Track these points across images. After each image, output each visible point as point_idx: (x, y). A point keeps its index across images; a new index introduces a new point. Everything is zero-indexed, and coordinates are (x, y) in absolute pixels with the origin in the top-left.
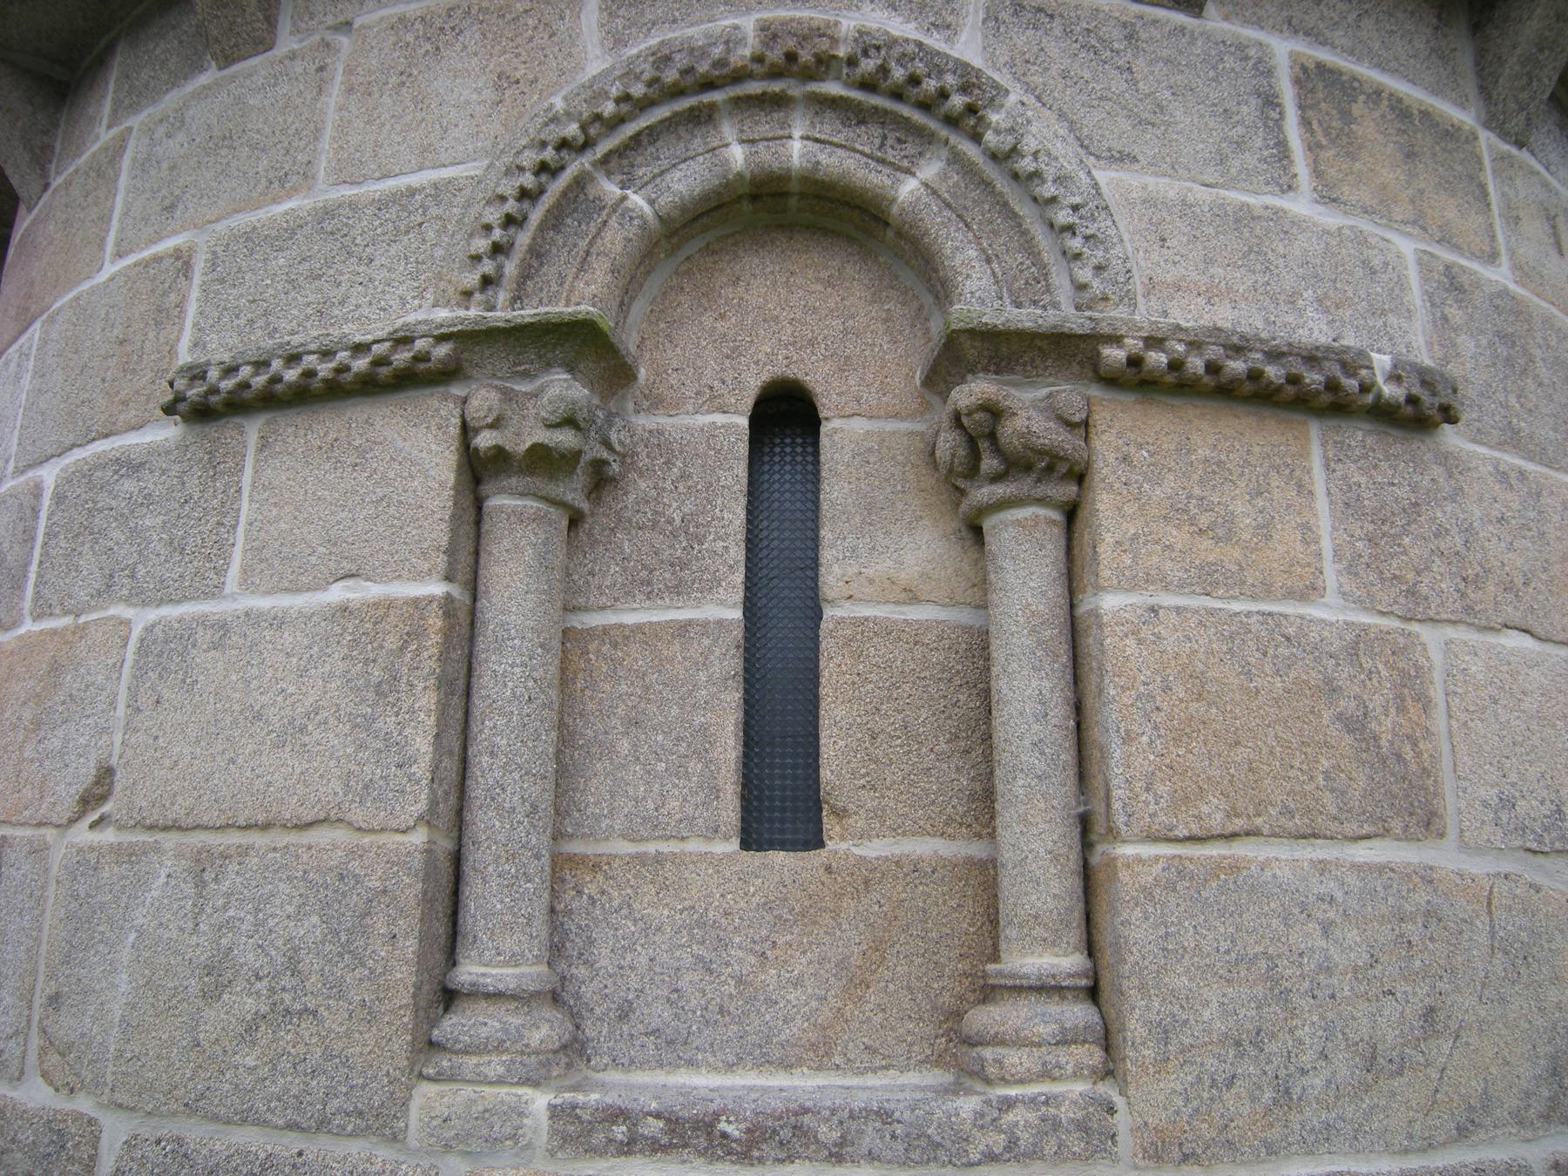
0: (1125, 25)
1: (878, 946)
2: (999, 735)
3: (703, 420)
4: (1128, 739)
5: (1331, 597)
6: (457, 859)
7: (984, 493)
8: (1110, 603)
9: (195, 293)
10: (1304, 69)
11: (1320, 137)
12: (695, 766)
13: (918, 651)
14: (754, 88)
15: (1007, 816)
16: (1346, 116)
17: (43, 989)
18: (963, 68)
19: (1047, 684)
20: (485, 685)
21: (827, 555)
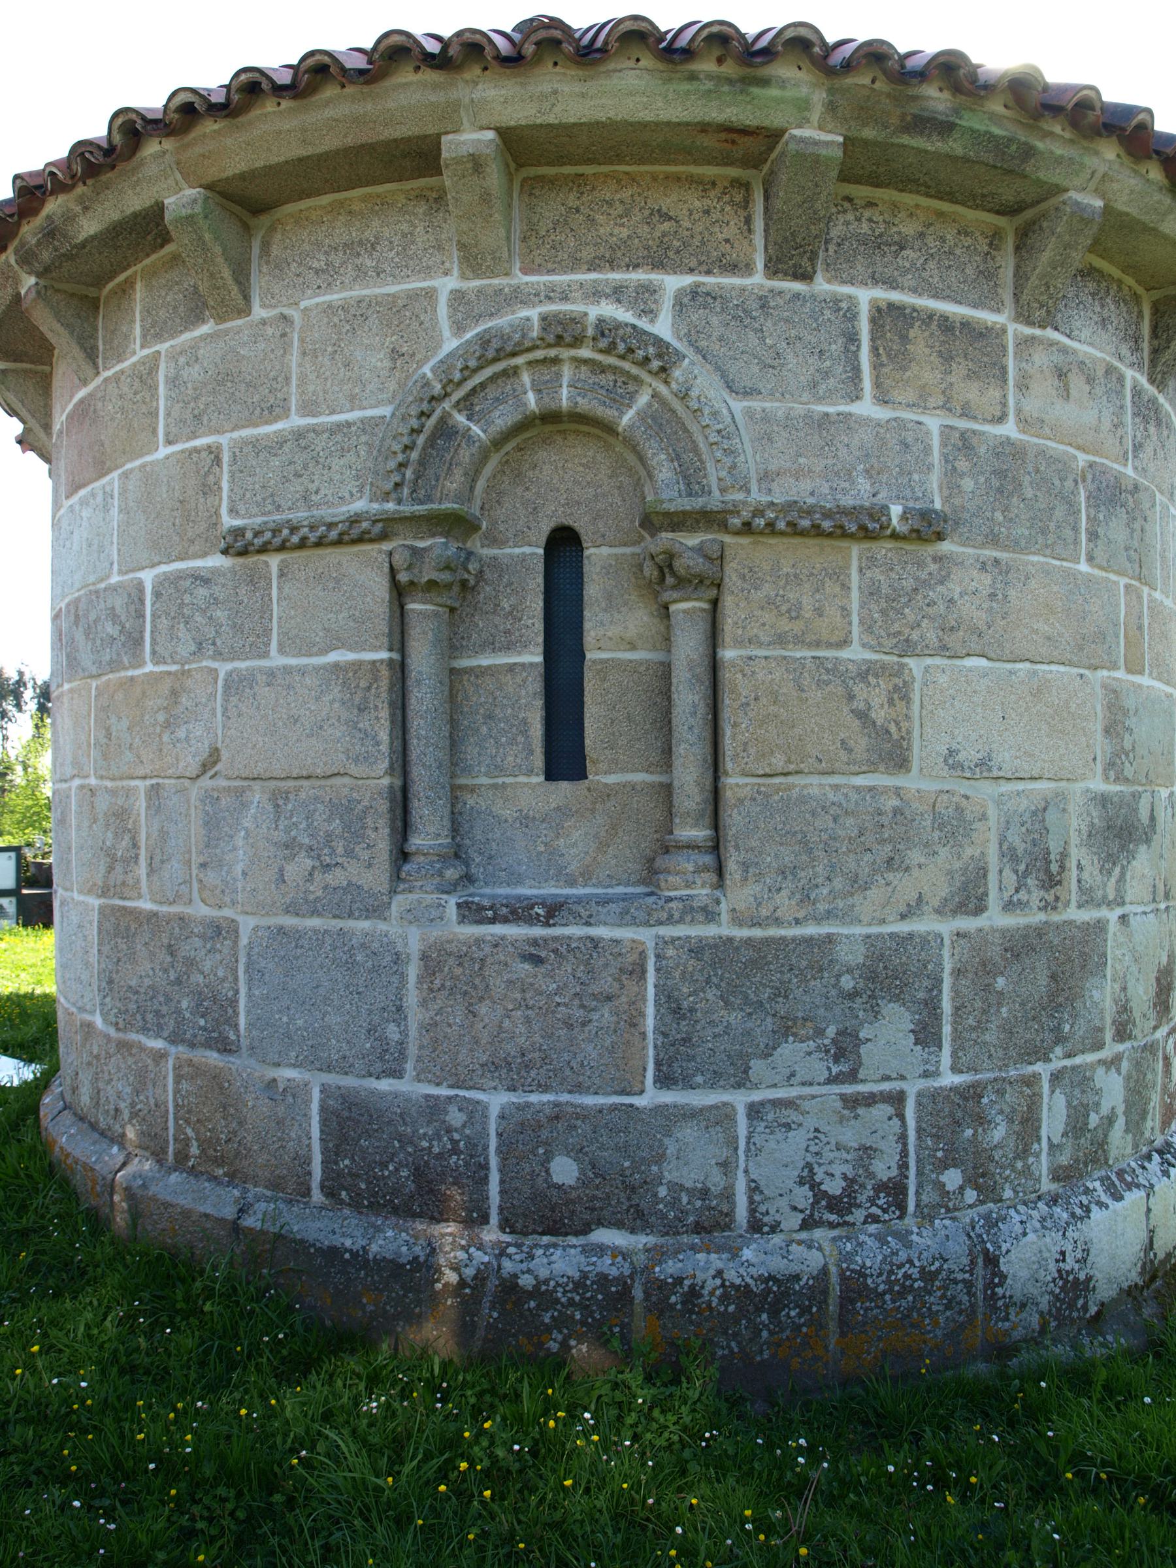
0: (761, 298)
1: (614, 827)
2: (674, 722)
3: (517, 551)
4: (735, 725)
5: (856, 644)
6: (405, 789)
7: (667, 596)
8: (728, 654)
9: (226, 477)
10: (879, 310)
11: (884, 359)
12: (521, 739)
13: (636, 676)
14: (539, 354)
15: (677, 763)
16: (904, 339)
17: (196, 860)
18: (658, 341)
19: (697, 698)
20: (413, 703)
21: (587, 625)
